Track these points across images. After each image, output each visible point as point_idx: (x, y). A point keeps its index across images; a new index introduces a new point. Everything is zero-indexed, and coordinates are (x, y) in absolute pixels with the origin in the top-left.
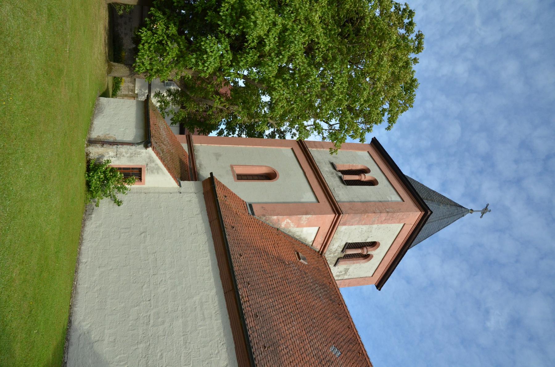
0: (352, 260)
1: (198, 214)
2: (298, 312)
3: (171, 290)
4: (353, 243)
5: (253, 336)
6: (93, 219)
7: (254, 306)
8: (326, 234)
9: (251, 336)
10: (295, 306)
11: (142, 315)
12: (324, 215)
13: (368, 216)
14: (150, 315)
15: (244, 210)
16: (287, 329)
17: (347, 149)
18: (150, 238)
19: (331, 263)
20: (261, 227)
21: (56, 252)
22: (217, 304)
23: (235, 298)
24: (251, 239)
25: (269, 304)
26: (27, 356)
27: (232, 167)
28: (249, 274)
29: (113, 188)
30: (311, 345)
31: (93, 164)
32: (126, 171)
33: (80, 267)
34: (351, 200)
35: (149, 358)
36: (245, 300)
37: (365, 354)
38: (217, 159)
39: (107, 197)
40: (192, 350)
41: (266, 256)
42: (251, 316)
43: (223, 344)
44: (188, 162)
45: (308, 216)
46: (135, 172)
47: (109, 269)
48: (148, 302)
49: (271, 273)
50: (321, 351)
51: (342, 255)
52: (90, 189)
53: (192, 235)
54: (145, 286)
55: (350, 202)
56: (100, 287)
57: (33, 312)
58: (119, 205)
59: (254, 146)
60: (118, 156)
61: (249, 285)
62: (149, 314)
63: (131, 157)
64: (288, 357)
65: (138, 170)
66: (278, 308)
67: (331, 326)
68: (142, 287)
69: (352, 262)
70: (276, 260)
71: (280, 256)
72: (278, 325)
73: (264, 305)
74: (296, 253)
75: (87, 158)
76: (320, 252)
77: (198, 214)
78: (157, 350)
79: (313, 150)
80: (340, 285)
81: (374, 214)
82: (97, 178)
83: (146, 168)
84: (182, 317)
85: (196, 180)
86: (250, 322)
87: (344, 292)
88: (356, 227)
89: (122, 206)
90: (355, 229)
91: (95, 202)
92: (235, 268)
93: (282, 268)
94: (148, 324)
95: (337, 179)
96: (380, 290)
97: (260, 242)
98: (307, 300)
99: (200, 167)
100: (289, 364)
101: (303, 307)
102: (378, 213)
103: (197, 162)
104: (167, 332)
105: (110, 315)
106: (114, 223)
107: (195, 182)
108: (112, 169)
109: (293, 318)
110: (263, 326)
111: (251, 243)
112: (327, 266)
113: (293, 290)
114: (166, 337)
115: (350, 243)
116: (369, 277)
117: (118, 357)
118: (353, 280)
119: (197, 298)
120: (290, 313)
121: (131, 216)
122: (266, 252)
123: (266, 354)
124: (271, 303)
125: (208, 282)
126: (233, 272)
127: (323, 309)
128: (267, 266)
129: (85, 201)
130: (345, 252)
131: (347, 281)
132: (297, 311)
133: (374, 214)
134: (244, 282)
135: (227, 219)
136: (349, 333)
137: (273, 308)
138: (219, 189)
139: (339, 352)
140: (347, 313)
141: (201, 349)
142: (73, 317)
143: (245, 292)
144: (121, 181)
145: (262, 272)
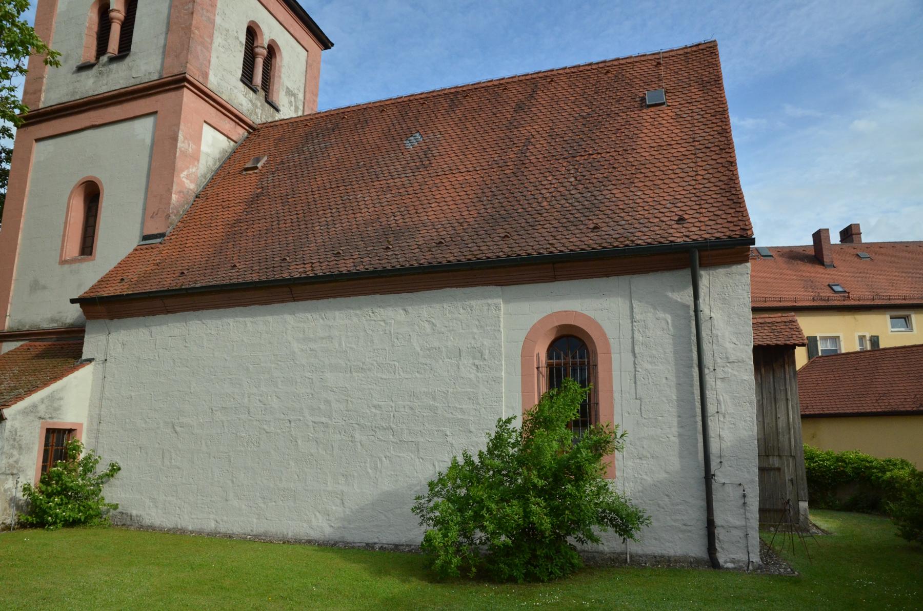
0: (274, 78)
1: (151, 332)
2: (343, 188)
3: (277, 387)
4: (243, 68)
5: (368, 264)
6: (139, 513)
7: (322, 257)
8: (218, 112)
9: (366, 267)
10: (332, 190)
11: (313, 434)
12: (183, 107)
13: (197, 28)
14: (313, 422)
15: (153, 250)
16: (366, 210)
17: (49, 29)
18: (185, 416)
19: (272, 116)
20: (188, 224)
21: (192, 568)
22: (309, 316)
23: (305, 284)
24: (209, 246)
25: (322, 231)
26: (347, 596)
27: (63, 262)
28: (268, 257)
29: (82, 479)
30: (397, 176)
31: (29, 517)
32: (51, 454)
33: (223, 530)
34: (161, 51)
35: (377, 425)
36: (310, 269)
37: (426, 95)
38: (44, 288)
39: (100, 490)
40: (374, 360)
41: (241, 224)
42: (336, 262)
43: (373, 313)
44: (45, 343)
45: (181, 137)
46: (55, 440)
47: (231, 485)
48: (293, 424)
49: (272, 220)
50: (409, 162)
51: (262, 93)
52: (83, 520)
53: (187, 345)
54: (265, 427)
55: (165, 53)
56: (260, 499)
57: (285, 595)
58: (119, 469)
59: (23, 214)
60: (15, 471)
61: (286, 260)
62: (311, 424)
63: (21, 448)
64: (409, 216)
65: (51, 436)
66: (331, 218)
67: (375, 139)
68: (267, 432)
69: (276, 79)
70: (251, 209)
71: (246, 200)
72: (357, 223)
73: (322, 240)
74: (244, 173)
75: (14, 529)
76: (250, 130)
77: (151, 332)
78: (367, 413)
79: (45, 98)
80: (312, 109)
81: (195, 15)
82: (59, 509)
83: (49, 420)
84: (322, 372)
85: (83, 331)
86: (348, 265)
87: (326, 103)
88: (214, 55)
89: (121, 465)
90: (218, 57)
91: (108, 511)
92: (254, 278)
93: (268, 200)
94: (326, 426)
95: (114, 66)
96: (333, 45)
97: (216, 231)
98: (327, 169)
99: (57, 321)
100: (419, 215)
101: (336, 177)
102: (193, 5)
103: (45, 325)
104: (343, 397)
105: (305, 483)
106: (151, 478)
107: (86, 333)
108: (42, 481)
109: (351, 197)
110: (355, 246)
111: (216, 246)
112: (277, 123)
113: (306, 188)
114: (350, 399)
115: (242, 75)
116: (308, 56)
117: (370, 471)
118: (307, 85)
119: (296, 346)
120: (342, 200)
121: (140, 448)
122: (234, 223)
123: (397, 248)
124: (322, 228)
125: (272, 327)
126: (260, 282)
127: (346, 146)
128: (260, 225)
129: (104, 528)
130: (258, 88)
131: (308, 96)
132: (340, 188)
133: (194, 15)
134: (281, 266)
135: (165, 283)
136: (390, 113)
137: (329, 227)
138: (105, 289)
139: (416, 134)
140: (359, 108)
141: (375, 347)
142: (302, 538)
143: (297, 267)
144: (71, 466)
145: (268, 235)
